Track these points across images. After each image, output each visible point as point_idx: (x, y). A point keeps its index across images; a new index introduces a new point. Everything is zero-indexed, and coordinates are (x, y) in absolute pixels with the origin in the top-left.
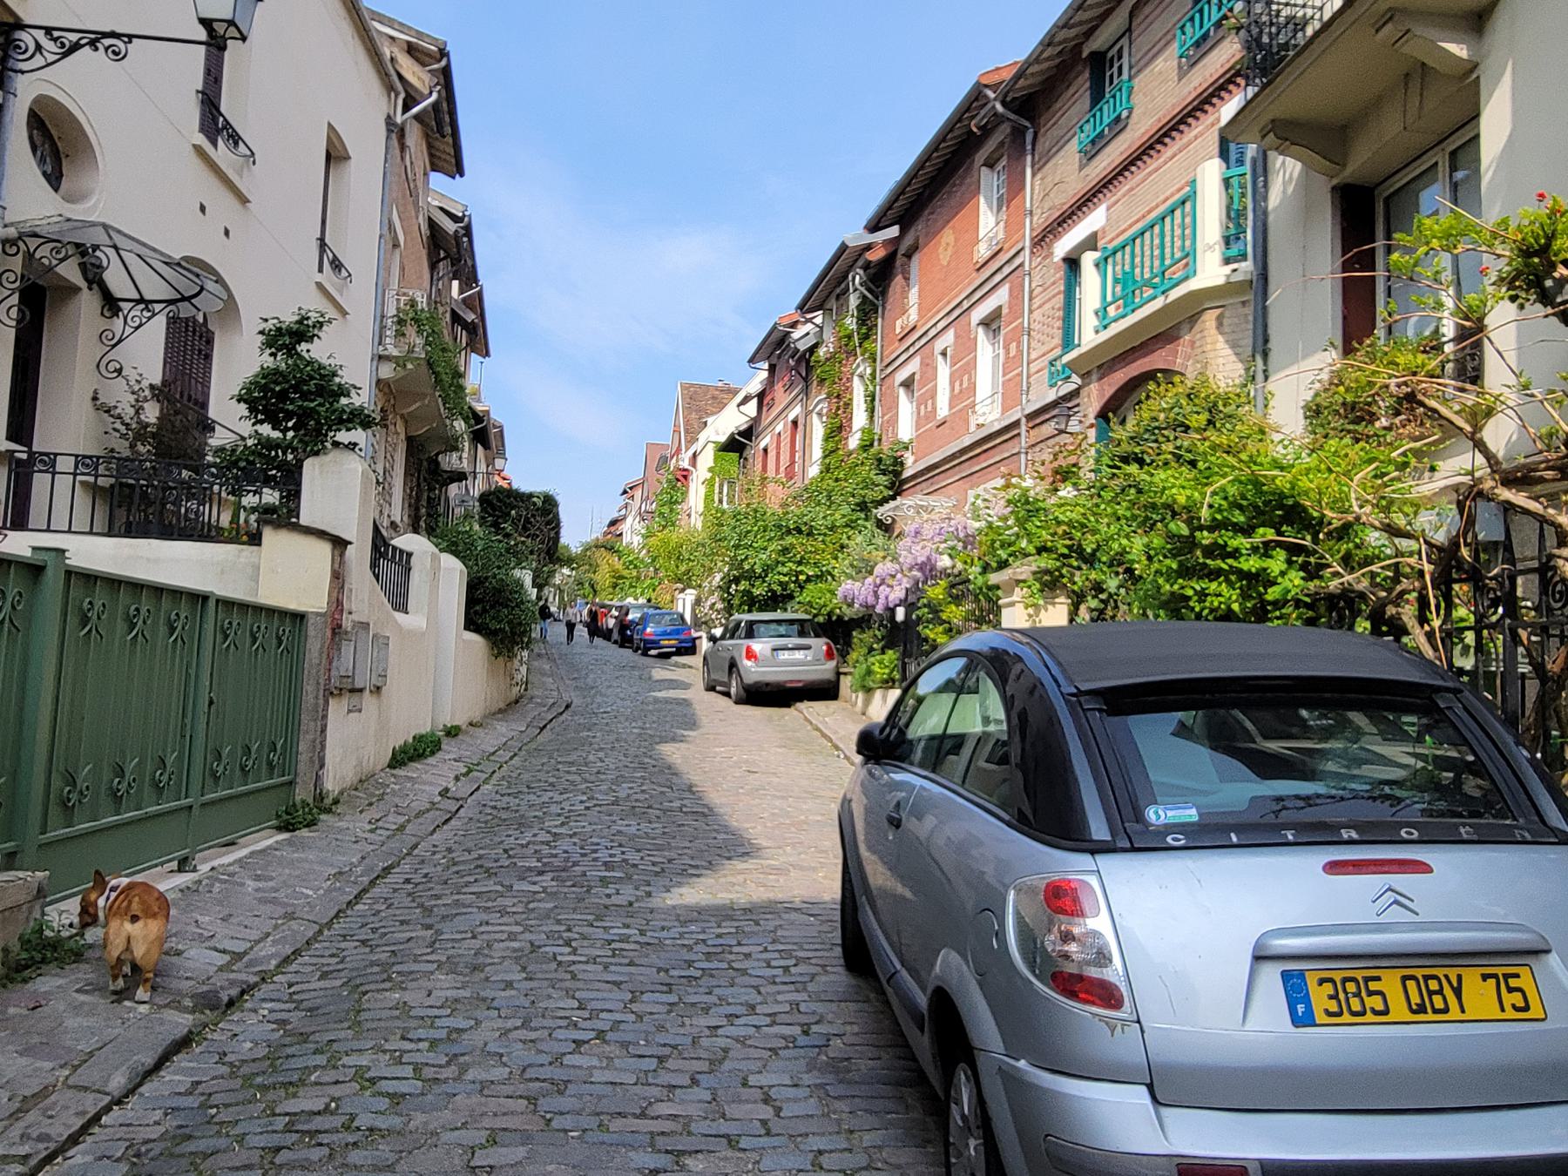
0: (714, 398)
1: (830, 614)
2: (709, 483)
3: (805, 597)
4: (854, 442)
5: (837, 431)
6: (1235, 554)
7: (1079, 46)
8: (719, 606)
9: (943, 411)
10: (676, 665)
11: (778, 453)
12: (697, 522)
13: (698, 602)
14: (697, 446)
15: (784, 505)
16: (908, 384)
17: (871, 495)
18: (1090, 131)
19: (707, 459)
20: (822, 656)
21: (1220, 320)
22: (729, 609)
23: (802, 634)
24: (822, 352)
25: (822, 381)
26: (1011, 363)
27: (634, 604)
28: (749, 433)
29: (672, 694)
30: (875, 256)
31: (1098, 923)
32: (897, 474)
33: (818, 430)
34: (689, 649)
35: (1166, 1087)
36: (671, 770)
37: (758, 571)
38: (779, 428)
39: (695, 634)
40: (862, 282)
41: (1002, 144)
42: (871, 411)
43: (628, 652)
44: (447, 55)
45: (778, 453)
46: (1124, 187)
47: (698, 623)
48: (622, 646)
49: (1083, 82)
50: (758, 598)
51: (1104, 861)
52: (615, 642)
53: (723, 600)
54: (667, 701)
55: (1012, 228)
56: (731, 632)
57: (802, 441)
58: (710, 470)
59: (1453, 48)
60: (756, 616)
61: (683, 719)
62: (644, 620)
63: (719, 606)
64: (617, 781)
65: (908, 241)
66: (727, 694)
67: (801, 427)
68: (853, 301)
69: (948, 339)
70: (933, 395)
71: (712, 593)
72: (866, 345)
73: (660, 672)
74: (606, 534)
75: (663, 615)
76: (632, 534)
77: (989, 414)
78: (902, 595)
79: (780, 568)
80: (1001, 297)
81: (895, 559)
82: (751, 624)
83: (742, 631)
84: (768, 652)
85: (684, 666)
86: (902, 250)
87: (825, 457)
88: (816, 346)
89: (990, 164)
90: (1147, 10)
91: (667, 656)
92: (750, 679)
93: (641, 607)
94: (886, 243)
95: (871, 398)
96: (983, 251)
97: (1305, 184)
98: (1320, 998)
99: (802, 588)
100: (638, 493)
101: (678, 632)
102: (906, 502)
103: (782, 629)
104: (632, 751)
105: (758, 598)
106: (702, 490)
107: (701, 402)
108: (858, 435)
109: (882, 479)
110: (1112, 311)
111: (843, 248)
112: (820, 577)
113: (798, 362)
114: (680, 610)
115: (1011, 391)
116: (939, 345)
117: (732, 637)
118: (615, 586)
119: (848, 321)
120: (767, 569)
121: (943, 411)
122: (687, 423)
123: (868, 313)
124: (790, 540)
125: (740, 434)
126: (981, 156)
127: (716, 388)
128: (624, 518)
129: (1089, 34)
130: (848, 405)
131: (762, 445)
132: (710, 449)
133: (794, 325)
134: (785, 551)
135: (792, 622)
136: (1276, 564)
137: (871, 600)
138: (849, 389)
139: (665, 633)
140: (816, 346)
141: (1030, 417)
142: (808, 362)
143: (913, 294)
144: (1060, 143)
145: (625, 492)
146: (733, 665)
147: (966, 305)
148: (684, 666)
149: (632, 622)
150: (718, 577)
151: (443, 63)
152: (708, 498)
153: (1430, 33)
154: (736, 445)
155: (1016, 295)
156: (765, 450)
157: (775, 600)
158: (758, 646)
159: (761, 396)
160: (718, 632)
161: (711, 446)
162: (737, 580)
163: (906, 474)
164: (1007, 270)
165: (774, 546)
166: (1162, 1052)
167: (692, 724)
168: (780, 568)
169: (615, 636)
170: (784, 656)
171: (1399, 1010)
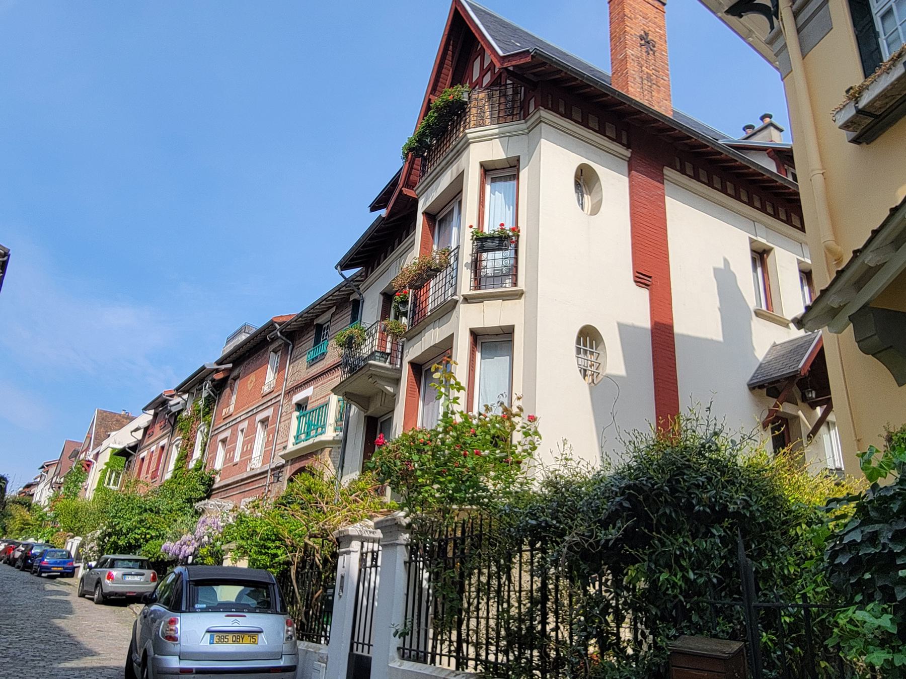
0: (117, 420)
1: (158, 558)
2: (104, 472)
3: (147, 547)
4: (192, 465)
5: (184, 457)
6: (269, 548)
7: (312, 320)
8: (96, 548)
9: (237, 459)
10: (60, 583)
11: (150, 462)
12: (90, 495)
13: (82, 545)
14: (102, 448)
15: (146, 496)
16: (224, 441)
17: (194, 495)
18: (312, 355)
19: (105, 457)
20: (149, 580)
21: (330, 452)
22: (102, 551)
23: (141, 567)
24: (184, 414)
25: (181, 429)
26: (268, 443)
27: (36, 542)
28: (135, 448)
29: (58, 597)
30: (219, 376)
31: (178, 626)
32: (210, 486)
33: (175, 454)
34: (71, 573)
35: (182, 656)
36: (60, 629)
37: (124, 531)
38: (153, 448)
39: (75, 565)
40: (212, 385)
41: (280, 345)
42: (204, 451)
43: (26, 575)
44: (9, 256)
45: (150, 462)
46: (321, 381)
47: (78, 558)
48: (23, 570)
49: (312, 334)
50: (118, 546)
51: (183, 614)
52: (18, 567)
53: (99, 545)
54: (56, 601)
55: (279, 383)
56: (101, 565)
57: (165, 459)
58: (106, 464)
59: (388, 388)
60: (117, 556)
61: (66, 609)
62: (43, 555)
63: (96, 548)
64: (34, 631)
65: (235, 373)
66: (92, 599)
67: (165, 451)
68: (204, 394)
69: (245, 425)
70: (234, 450)
71: (92, 540)
72: (207, 417)
73: (50, 586)
74: (21, 493)
75: (56, 552)
76: (42, 495)
77: (257, 464)
78: (193, 551)
79: (136, 531)
80: (269, 412)
81: (193, 533)
82: (113, 561)
83: (108, 564)
84: (120, 576)
85: (65, 584)
86: (232, 377)
87: (175, 470)
88: (182, 410)
89: (275, 352)
90: (337, 317)
91: (54, 577)
92: (106, 590)
93: (41, 545)
94: (225, 369)
95: (204, 445)
96: (266, 389)
97: (359, 414)
98: (216, 639)
99: (147, 541)
100: (52, 470)
101: (64, 563)
102: (211, 503)
103: (131, 564)
104: (39, 621)
105: (118, 546)
106: (99, 475)
107: (110, 422)
108: (194, 462)
109: (202, 488)
110: (303, 437)
111: (203, 368)
112: (157, 537)
113: (171, 416)
114: (68, 548)
115: (266, 457)
116: (241, 426)
117: (101, 567)
118: (22, 529)
119: (200, 403)
120: (130, 530)
121: (237, 459)
122: (97, 433)
123: (210, 402)
124: (145, 515)
125: (129, 448)
126: (272, 347)
127: (120, 415)
128: (38, 484)
129: (317, 316)
130: (193, 445)
131: (142, 456)
132: (109, 451)
133: (172, 396)
134: (141, 521)
135: (137, 561)
136: (279, 552)
137: (177, 552)
138: (195, 437)
139: (55, 563)
140: (182, 410)
141: (272, 470)
142: (176, 417)
143: (234, 398)
144: (301, 355)
145: (43, 467)
146: (99, 582)
147: (255, 411)
148: (65, 584)
149: (34, 554)
150: (99, 532)
151: (6, 258)
152: (101, 481)
153: (382, 383)
154: (126, 453)
155: (275, 412)
156: (143, 459)
157: (130, 548)
158: (115, 573)
159: (146, 429)
160: (93, 564)
161: (109, 450)
162: (110, 535)
163: (215, 486)
164: (274, 401)
165: (137, 518)
166: (183, 649)
167: (71, 612)
168: (136, 531)
169: (19, 563)
170: (129, 578)
171: (230, 641)
